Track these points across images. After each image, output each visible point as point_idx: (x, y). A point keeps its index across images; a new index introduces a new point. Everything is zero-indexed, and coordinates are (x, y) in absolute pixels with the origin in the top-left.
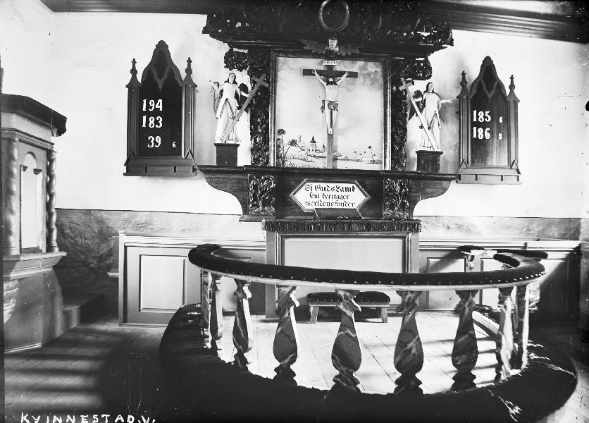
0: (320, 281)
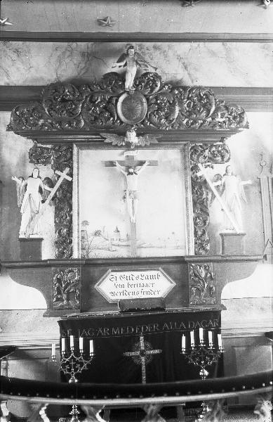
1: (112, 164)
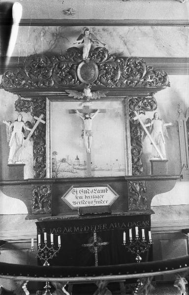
0: (38, 277)
1: (74, 112)
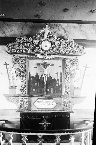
0: (16, 132)
1: (38, 64)
